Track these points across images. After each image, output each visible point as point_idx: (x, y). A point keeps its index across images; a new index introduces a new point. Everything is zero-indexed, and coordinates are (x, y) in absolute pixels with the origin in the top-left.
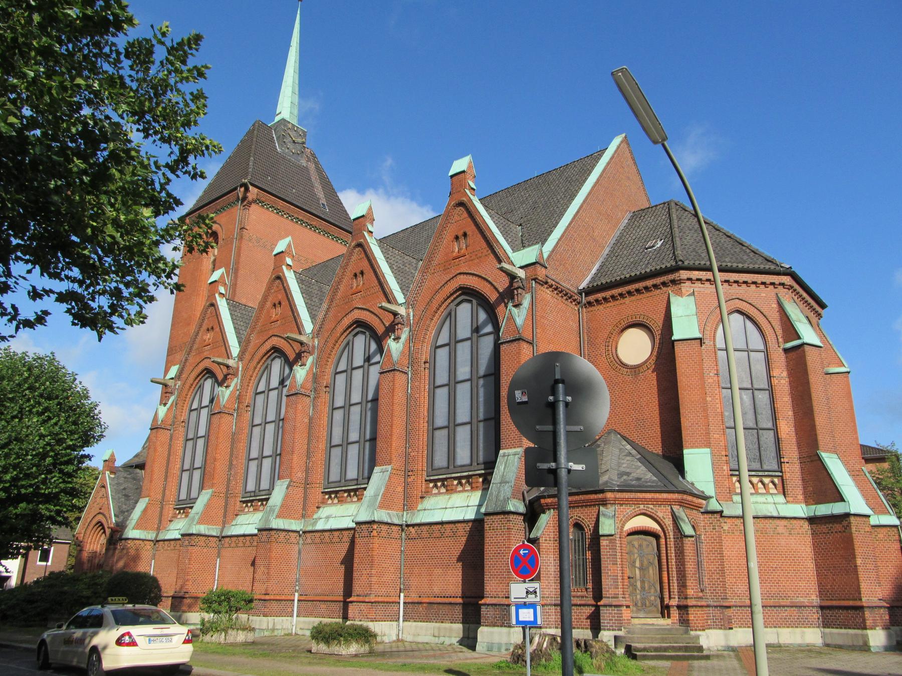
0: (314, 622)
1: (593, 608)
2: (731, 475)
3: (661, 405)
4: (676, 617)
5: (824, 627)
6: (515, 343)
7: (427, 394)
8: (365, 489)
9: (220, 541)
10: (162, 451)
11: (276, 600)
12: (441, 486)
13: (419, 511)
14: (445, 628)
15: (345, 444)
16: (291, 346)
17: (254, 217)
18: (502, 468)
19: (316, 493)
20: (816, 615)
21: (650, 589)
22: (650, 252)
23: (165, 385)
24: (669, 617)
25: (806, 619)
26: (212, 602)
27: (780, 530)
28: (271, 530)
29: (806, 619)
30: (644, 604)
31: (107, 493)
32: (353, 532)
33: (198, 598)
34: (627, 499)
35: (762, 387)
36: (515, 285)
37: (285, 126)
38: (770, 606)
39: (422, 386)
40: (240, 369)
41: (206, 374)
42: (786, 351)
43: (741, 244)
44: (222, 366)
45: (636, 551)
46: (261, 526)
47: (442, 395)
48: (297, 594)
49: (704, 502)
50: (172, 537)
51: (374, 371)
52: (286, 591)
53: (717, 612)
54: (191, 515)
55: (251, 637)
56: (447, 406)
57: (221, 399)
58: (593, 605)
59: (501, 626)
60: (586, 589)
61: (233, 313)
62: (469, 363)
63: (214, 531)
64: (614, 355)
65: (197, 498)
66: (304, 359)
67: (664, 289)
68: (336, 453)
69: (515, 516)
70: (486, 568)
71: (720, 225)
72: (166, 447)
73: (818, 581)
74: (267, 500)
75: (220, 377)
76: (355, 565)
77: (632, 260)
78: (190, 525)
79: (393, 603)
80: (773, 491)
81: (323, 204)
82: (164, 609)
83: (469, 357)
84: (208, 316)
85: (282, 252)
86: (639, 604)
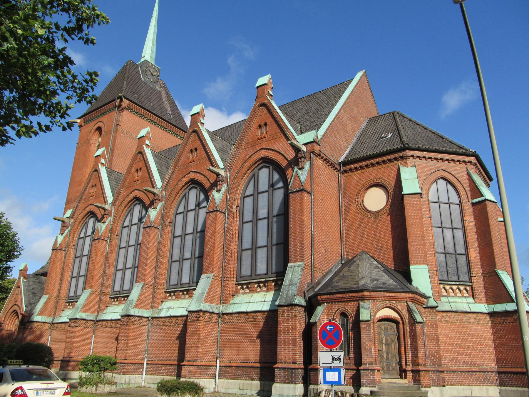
0: (157, 379)
1: (355, 372)
2: (440, 284)
3: (393, 237)
4: (410, 378)
5: (501, 386)
6: (300, 193)
7: (237, 227)
8: (194, 290)
9: (95, 323)
10: (59, 265)
11: (132, 363)
12: (246, 288)
13: (231, 304)
14: (248, 384)
15: (182, 260)
16: (147, 196)
17: (126, 118)
18: (290, 275)
19: (161, 293)
20: (495, 378)
21: (392, 358)
22: (385, 140)
23: (63, 222)
24: (406, 378)
25: (489, 380)
26: (85, 365)
28: (130, 316)
29: (489, 380)
30: (388, 369)
31: (21, 291)
32: (185, 318)
33: (79, 361)
34: (378, 297)
35: (458, 227)
36: (300, 156)
37: (147, 64)
38: (466, 371)
39: (235, 221)
40: (113, 211)
41: (90, 215)
42: (473, 204)
43: (442, 138)
44: (101, 210)
45: (383, 332)
47: (248, 228)
48: (146, 360)
49: (425, 300)
50: (63, 321)
51: (202, 213)
52: (139, 357)
53: (435, 374)
54: (76, 306)
55: (113, 389)
56: (251, 235)
57: (100, 230)
58: (354, 369)
59: (289, 383)
60: (350, 358)
62: (267, 207)
63: (91, 316)
64: (362, 204)
65: (81, 296)
66: (155, 205)
67: (396, 162)
68: (175, 266)
69: (299, 308)
70: (279, 343)
71: (427, 126)
72: (62, 262)
73: (496, 355)
74: (128, 296)
75: (99, 217)
76: (187, 340)
77: (372, 145)
78: (75, 313)
79: (212, 366)
81: (169, 114)
82: (53, 371)
83: (267, 203)
84: (93, 178)
85: (144, 136)
86: (385, 369)
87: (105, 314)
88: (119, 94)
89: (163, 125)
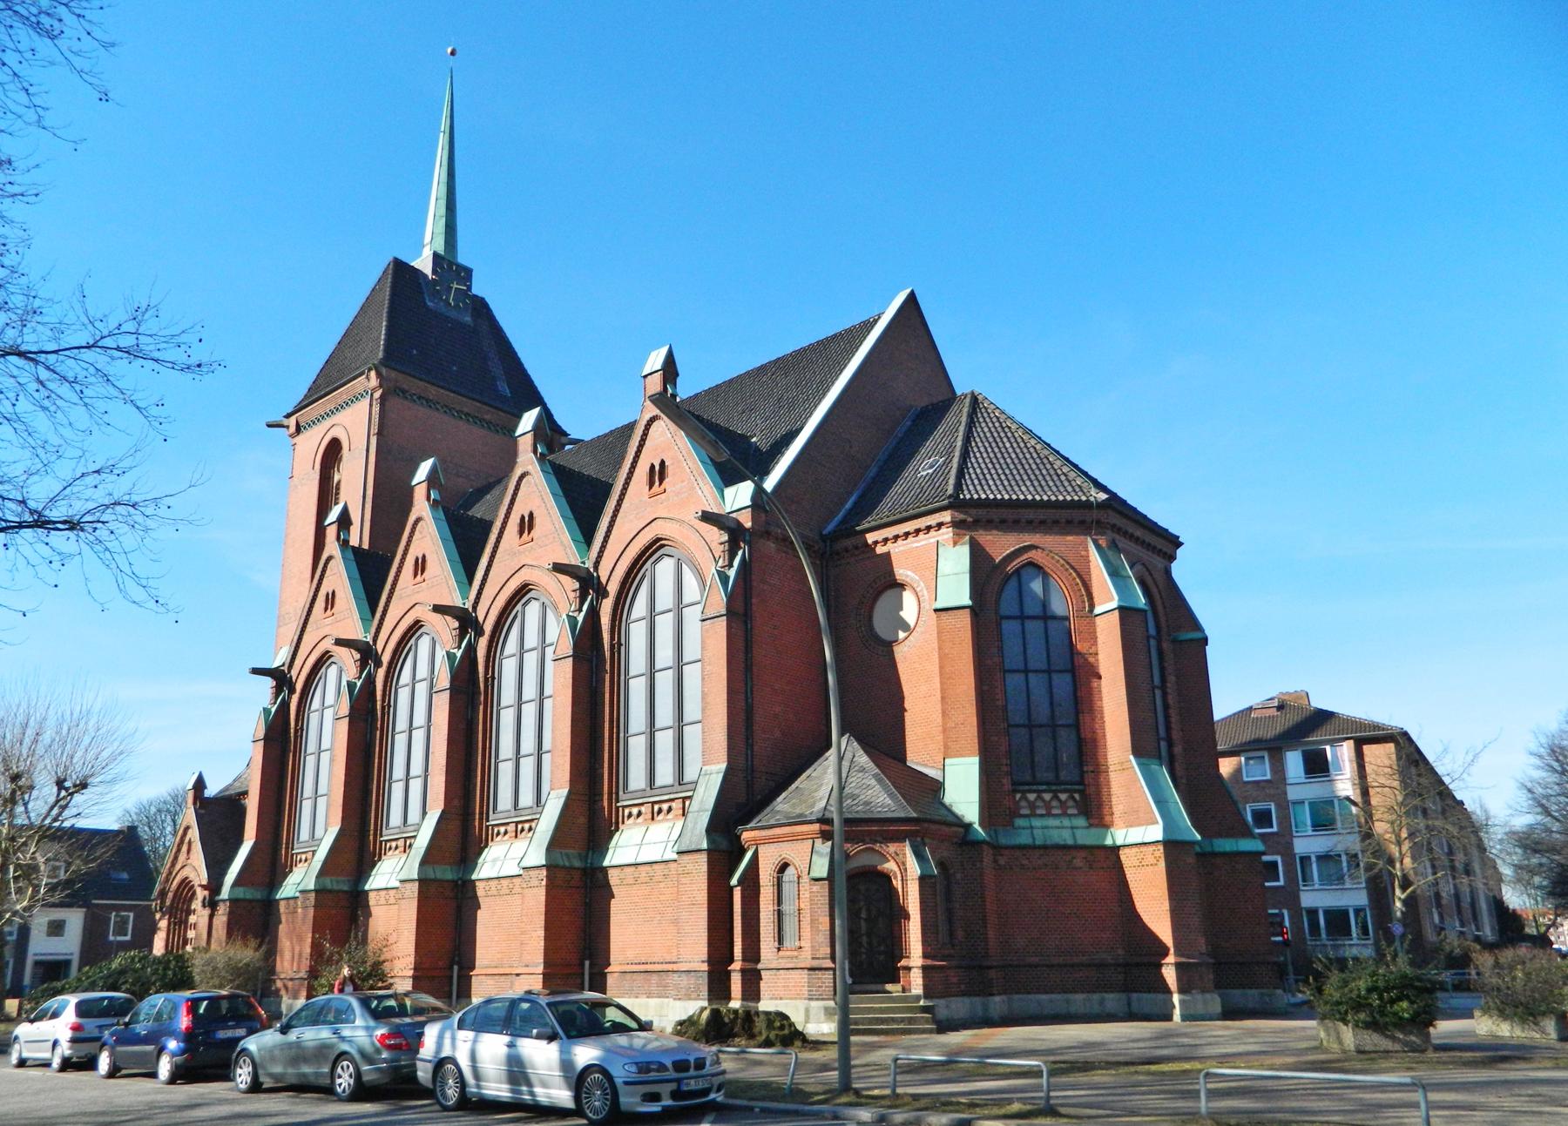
27: (1078, 862)
89: (487, 417)
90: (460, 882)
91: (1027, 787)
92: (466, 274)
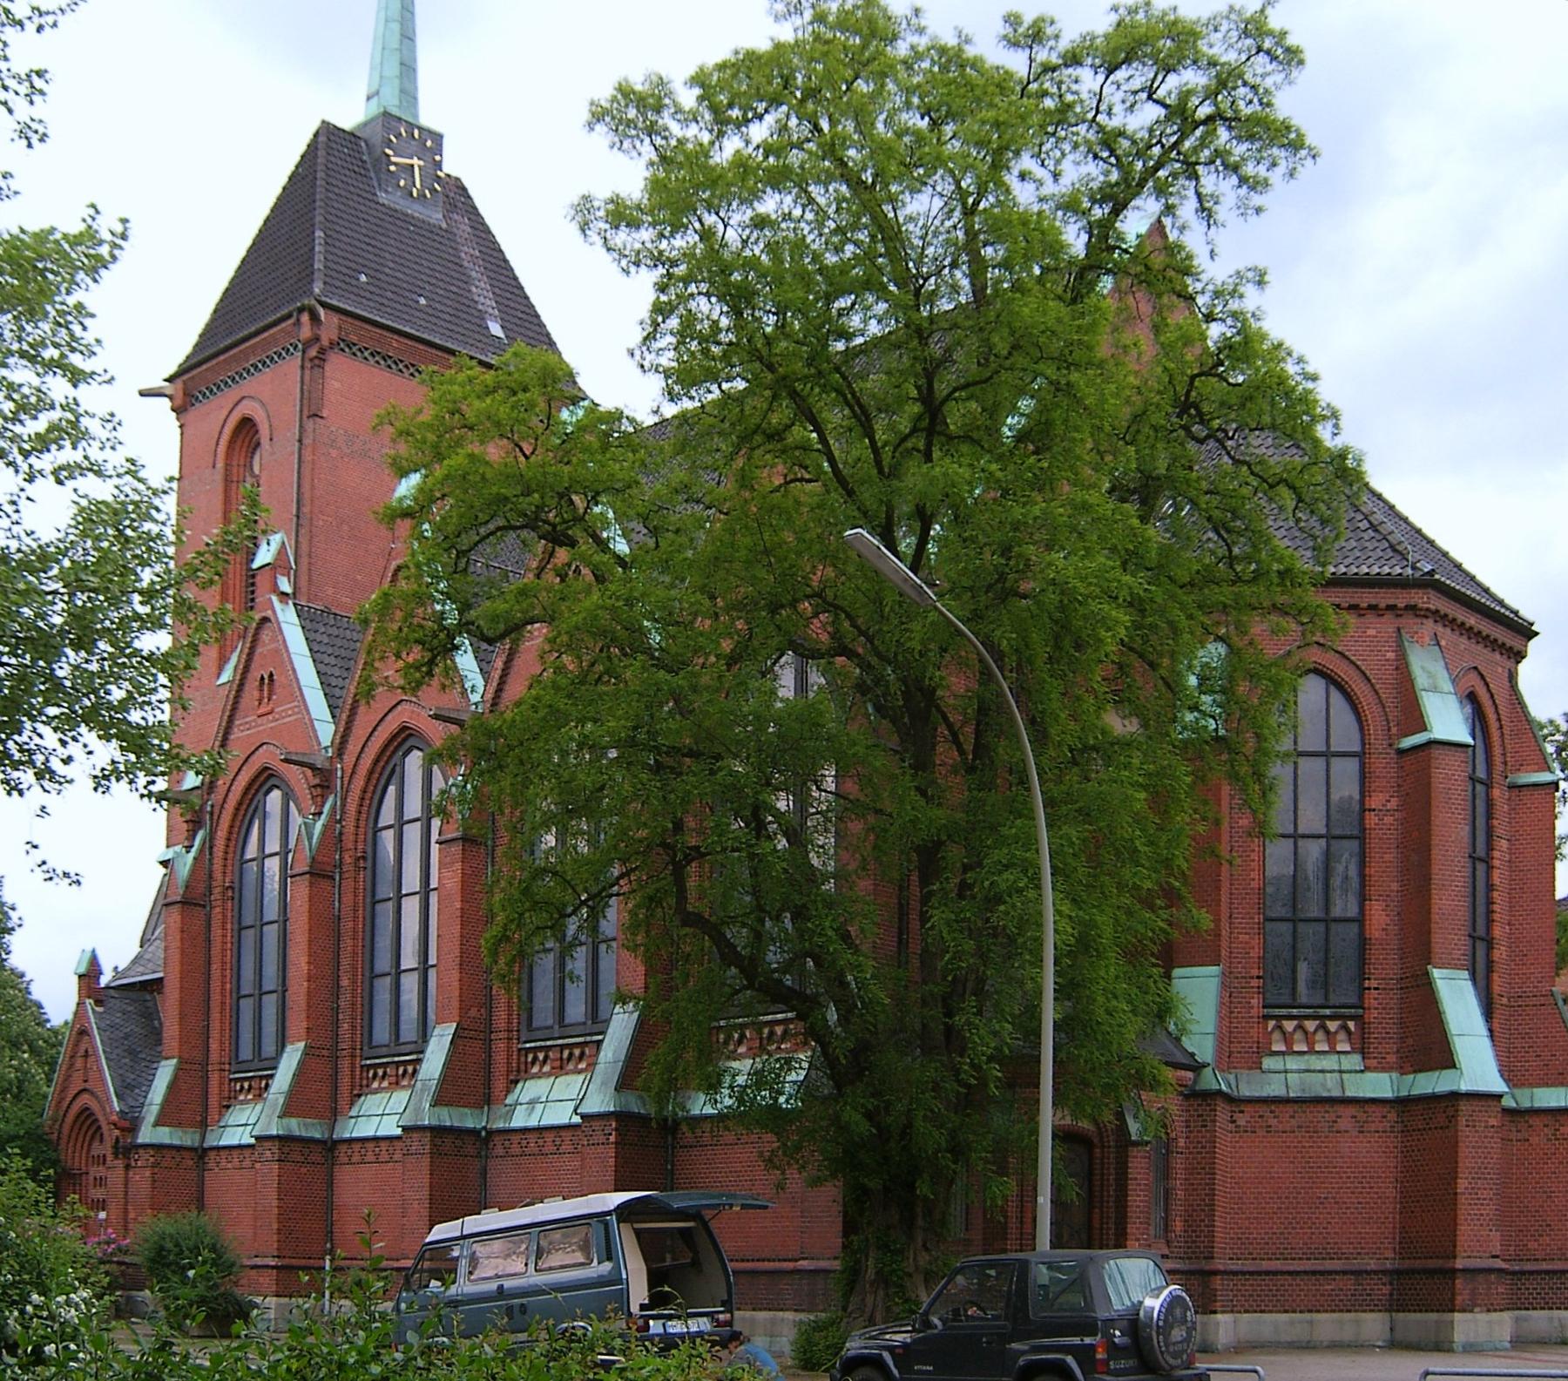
46: (407, 1121)
50: (235, 1142)
61: (312, 636)
80: (1344, 1046)
87: (353, 1120)
88: (451, 501)
90: (483, 1133)
91: (1284, 1012)
92: (430, 144)
